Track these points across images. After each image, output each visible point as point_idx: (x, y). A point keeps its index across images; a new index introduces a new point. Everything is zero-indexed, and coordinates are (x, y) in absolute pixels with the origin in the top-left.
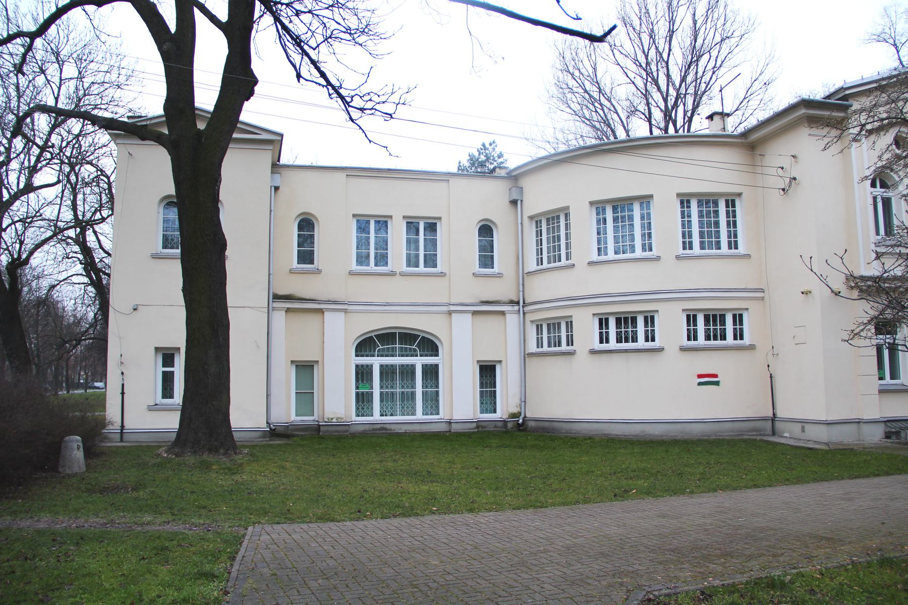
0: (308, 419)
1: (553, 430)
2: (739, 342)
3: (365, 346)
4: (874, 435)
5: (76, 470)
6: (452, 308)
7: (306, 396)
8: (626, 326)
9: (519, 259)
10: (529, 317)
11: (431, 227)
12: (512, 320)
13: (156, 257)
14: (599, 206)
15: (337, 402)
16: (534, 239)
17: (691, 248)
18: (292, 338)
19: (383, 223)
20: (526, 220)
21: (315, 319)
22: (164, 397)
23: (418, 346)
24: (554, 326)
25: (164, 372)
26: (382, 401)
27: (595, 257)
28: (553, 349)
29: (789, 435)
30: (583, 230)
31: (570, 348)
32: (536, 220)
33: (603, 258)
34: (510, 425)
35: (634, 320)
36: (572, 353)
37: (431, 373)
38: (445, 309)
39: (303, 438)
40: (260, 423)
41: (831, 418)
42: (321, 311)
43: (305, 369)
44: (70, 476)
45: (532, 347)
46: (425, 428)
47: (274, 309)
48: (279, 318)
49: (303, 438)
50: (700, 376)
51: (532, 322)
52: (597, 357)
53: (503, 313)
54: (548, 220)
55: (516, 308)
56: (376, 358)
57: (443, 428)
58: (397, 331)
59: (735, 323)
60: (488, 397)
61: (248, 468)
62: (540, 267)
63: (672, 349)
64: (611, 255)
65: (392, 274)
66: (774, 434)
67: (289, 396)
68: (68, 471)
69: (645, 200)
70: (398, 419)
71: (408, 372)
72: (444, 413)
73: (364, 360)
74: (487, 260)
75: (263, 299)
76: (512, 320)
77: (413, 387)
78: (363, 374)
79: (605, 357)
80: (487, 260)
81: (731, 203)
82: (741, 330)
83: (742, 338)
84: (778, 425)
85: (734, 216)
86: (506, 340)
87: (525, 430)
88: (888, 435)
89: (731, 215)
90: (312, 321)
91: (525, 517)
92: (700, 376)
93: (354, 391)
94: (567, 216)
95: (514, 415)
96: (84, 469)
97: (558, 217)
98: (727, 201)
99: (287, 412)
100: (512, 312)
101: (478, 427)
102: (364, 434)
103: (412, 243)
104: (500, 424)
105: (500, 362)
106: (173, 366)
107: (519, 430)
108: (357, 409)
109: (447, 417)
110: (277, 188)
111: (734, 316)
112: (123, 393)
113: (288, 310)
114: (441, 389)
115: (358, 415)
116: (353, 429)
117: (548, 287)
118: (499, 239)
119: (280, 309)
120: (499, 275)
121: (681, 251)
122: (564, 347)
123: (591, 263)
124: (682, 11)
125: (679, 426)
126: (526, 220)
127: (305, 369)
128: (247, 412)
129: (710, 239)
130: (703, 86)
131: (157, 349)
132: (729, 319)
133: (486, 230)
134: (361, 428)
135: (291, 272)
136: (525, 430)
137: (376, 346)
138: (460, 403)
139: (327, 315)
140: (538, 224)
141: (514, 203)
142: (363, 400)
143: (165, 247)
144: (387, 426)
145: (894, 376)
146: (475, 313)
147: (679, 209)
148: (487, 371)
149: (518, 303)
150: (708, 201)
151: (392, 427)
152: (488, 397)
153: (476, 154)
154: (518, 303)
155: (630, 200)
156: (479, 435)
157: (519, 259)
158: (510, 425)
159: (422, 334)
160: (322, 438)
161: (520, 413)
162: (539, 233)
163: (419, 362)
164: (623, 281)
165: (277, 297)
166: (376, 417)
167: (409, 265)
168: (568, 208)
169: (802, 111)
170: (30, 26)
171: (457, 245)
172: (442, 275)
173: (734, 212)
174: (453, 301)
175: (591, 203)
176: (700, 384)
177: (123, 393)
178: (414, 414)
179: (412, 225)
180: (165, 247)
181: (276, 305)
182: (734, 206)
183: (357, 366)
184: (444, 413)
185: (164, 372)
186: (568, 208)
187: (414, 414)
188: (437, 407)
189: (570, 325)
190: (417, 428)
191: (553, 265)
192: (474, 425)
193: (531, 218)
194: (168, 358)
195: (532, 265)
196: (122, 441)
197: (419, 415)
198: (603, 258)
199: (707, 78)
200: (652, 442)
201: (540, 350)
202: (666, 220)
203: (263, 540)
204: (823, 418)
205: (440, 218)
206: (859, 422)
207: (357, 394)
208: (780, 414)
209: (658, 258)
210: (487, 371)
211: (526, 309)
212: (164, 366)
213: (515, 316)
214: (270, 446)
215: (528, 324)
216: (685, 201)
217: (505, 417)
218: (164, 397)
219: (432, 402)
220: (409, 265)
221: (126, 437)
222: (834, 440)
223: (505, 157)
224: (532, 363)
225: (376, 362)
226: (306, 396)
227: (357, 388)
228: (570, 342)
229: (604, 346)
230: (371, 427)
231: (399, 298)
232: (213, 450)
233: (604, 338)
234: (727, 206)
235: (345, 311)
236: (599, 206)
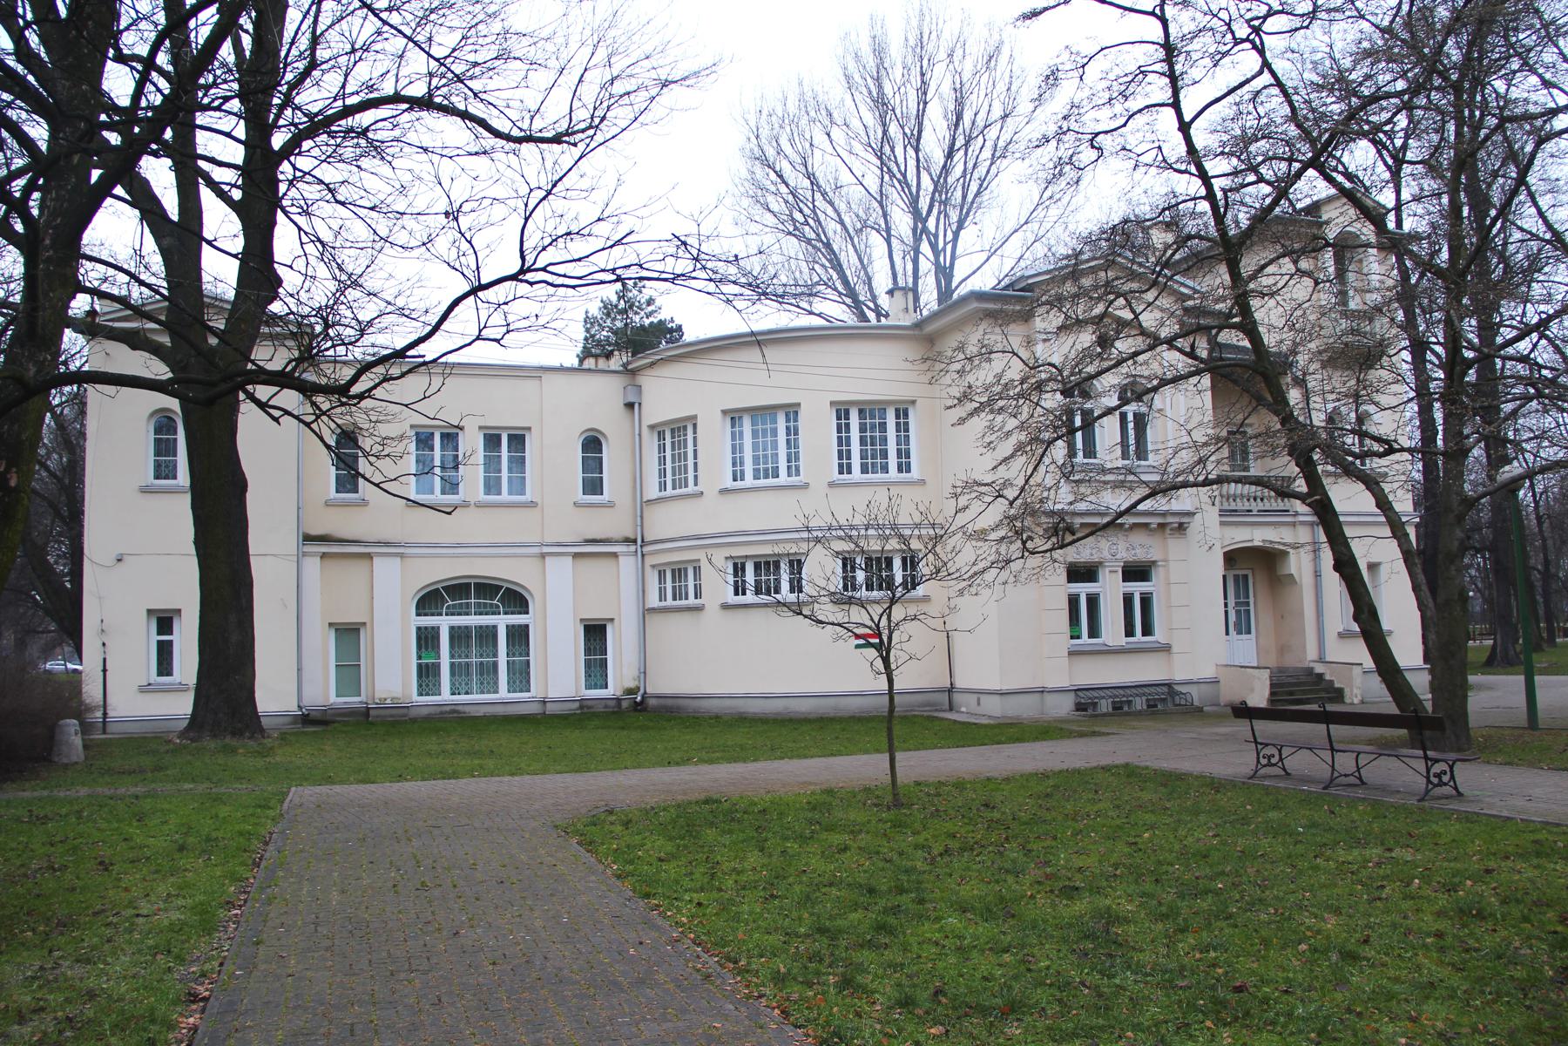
0: (352, 701)
1: (679, 709)
3: (429, 601)
4: (1063, 707)
5: (74, 759)
6: (546, 550)
7: (349, 672)
8: (767, 575)
9: (638, 481)
10: (650, 561)
11: (518, 440)
12: (627, 565)
13: (146, 490)
14: (733, 417)
15: (391, 676)
16: (657, 455)
17: (849, 472)
18: (328, 593)
19: (450, 438)
20: (645, 431)
21: (359, 568)
22: (160, 674)
23: (502, 600)
24: (679, 573)
25: (159, 642)
26: (453, 674)
27: (729, 483)
28: (678, 603)
29: (967, 709)
30: (714, 448)
31: (698, 601)
32: (658, 430)
33: (739, 484)
34: (625, 704)
35: (777, 565)
36: (699, 609)
37: (519, 636)
38: (536, 550)
39: (346, 723)
40: (291, 706)
41: (1005, 687)
42: (369, 556)
43: (348, 634)
44: (66, 766)
45: (653, 601)
47: (305, 554)
48: (312, 566)
49: (346, 723)
51: (653, 566)
52: (730, 613)
53: (615, 555)
54: (673, 431)
55: (633, 548)
56: (444, 617)
57: (534, 709)
58: (472, 581)
60: (596, 669)
61: (280, 751)
62: (663, 494)
64: (749, 481)
65: (465, 504)
66: (951, 709)
67: (326, 667)
68: (65, 761)
69: (792, 411)
71: (489, 634)
72: (536, 691)
74: (593, 486)
75: (291, 542)
76: (627, 565)
77: (495, 655)
78: (427, 639)
79: (741, 613)
80: (593, 486)
81: (902, 413)
84: (957, 697)
85: (907, 430)
86: (618, 591)
87: (645, 710)
88: (1080, 707)
89: (902, 428)
90: (356, 570)
91: (569, 778)
93: (414, 662)
94: (695, 426)
95: (630, 691)
96: (82, 757)
97: (685, 428)
98: (897, 410)
99: (325, 692)
100: (627, 554)
101: (581, 707)
102: (428, 719)
103: (492, 464)
104: (612, 703)
105: (612, 620)
106: (171, 633)
107: (636, 710)
108: (420, 686)
109: (540, 695)
112: (105, 671)
113: (324, 556)
114: (532, 658)
115: (420, 694)
116: (413, 713)
117: (667, 522)
118: (610, 455)
120: (610, 505)
121: (836, 475)
122: (692, 601)
123: (724, 491)
124: (939, 69)
125: (832, 701)
126: (645, 431)
127: (348, 634)
128: (274, 694)
129: (874, 460)
130: (974, 188)
131: (150, 612)
133: (592, 444)
134: (425, 711)
135: (328, 504)
136: (645, 710)
137: (444, 601)
138: (558, 675)
139: (376, 560)
140: (661, 436)
141: (630, 406)
142: (428, 675)
143: (157, 477)
144: (460, 708)
145: (1147, 631)
146: (576, 555)
147: (835, 422)
148: (595, 633)
149: (635, 541)
150: (871, 411)
151: (467, 709)
152: (596, 669)
153: (614, 299)
154: (635, 541)
155: (773, 409)
156: (582, 716)
157: (638, 481)
158: (625, 704)
159: (506, 585)
160: (372, 724)
161: (638, 688)
162: (662, 449)
163: (502, 622)
164: (767, 516)
165: (308, 538)
166: (446, 696)
167: (488, 492)
168: (695, 417)
169: (975, 305)
171: (554, 462)
172: (532, 505)
173: (906, 424)
174: (548, 540)
175: (725, 412)
176: (858, 646)
177: (105, 671)
178: (496, 692)
179: (492, 441)
180: (157, 477)
182: (906, 415)
183: (419, 629)
184: (536, 691)
185: (159, 642)
186: (695, 417)
187: (496, 692)
188: (528, 682)
190: (500, 710)
191: (678, 491)
192: (577, 705)
193: (652, 427)
194: (165, 622)
195: (652, 491)
196: (104, 732)
197: (503, 693)
198: (739, 484)
199: (982, 170)
200: (791, 720)
201: (663, 604)
202: (818, 433)
203: (302, 794)
204: (997, 687)
205: (529, 429)
206: (1042, 691)
207: (420, 666)
208: (959, 684)
209: (806, 486)
210: (595, 633)
211: (646, 549)
212: (159, 633)
213: (632, 559)
214: (305, 733)
215: (648, 569)
216: (842, 412)
217: (619, 693)
218: (160, 674)
219: (521, 675)
220: (488, 492)
221: (110, 728)
222: (1010, 713)
223: (658, 303)
224: (654, 622)
225: (444, 623)
226: (349, 672)
227: (419, 657)
229: (740, 599)
230: (439, 709)
231: (476, 539)
232: (237, 733)
233: (739, 589)
234: (898, 417)
235: (402, 556)
236: (733, 417)
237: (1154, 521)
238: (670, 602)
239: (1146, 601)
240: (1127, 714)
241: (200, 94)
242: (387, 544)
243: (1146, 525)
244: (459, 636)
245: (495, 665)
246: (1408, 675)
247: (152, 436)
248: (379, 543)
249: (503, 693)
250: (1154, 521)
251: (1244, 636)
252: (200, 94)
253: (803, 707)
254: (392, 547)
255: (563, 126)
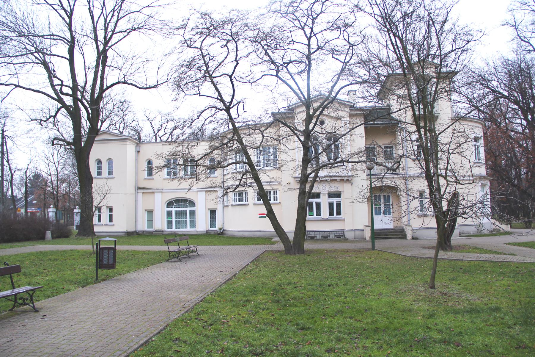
2: (275, 201)
3: (170, 204)
7: (150, 222)
15: (160, 223)
37: (193, 213)
42: (153, 193)
46: (189, 233)
48: (140, 195)
50: (260, 214)
59: (274, 194)
60: (213, 223)
63: (251, 205)
70: (181, 230)
73: (169, 209)
78: (169, 214)
82: (277, 197)
83: (277, 200)
90: (151, 196)
92: (260, 214)
95: (221, 229)
110: (139, 152)
111: (274, 192)
113: (143, 193)
116: (164, 233)
119: (140, 192)
132: (272, 193)
134: (167, 233)
138: (202, 224)
139: (155, 194)
142: (169, 223)
146: (206, 191)
148: (213, 212)
152: (213, 223)
156: (208, 234)
163: (188, 209)
165: (140, 188)
166: (174, 229)
170: (54, 115)
181: (139, 191)
189: (246, 194)
197: (188, 228)
224: (225, 208)
225: (173, 210)
226: (150, 222)
228: (246, 200)
235: (162, 192)
237: (338, 179)
238: (238, 203)
239: (339, 205)
240: (328, 240)
241: (401, 92)
242: (159, 189)
243: (326, 180)
244: (177, 213)
245: (172, 221)
246: (287, 233)
247: (97, 165)
248: (157, 189)
249: (188, 228)
250: (338, 179)
251: (378, 216)
252: (401, 92)
253: (246, 234)
254: (160, 190)
255: (156, 84)
